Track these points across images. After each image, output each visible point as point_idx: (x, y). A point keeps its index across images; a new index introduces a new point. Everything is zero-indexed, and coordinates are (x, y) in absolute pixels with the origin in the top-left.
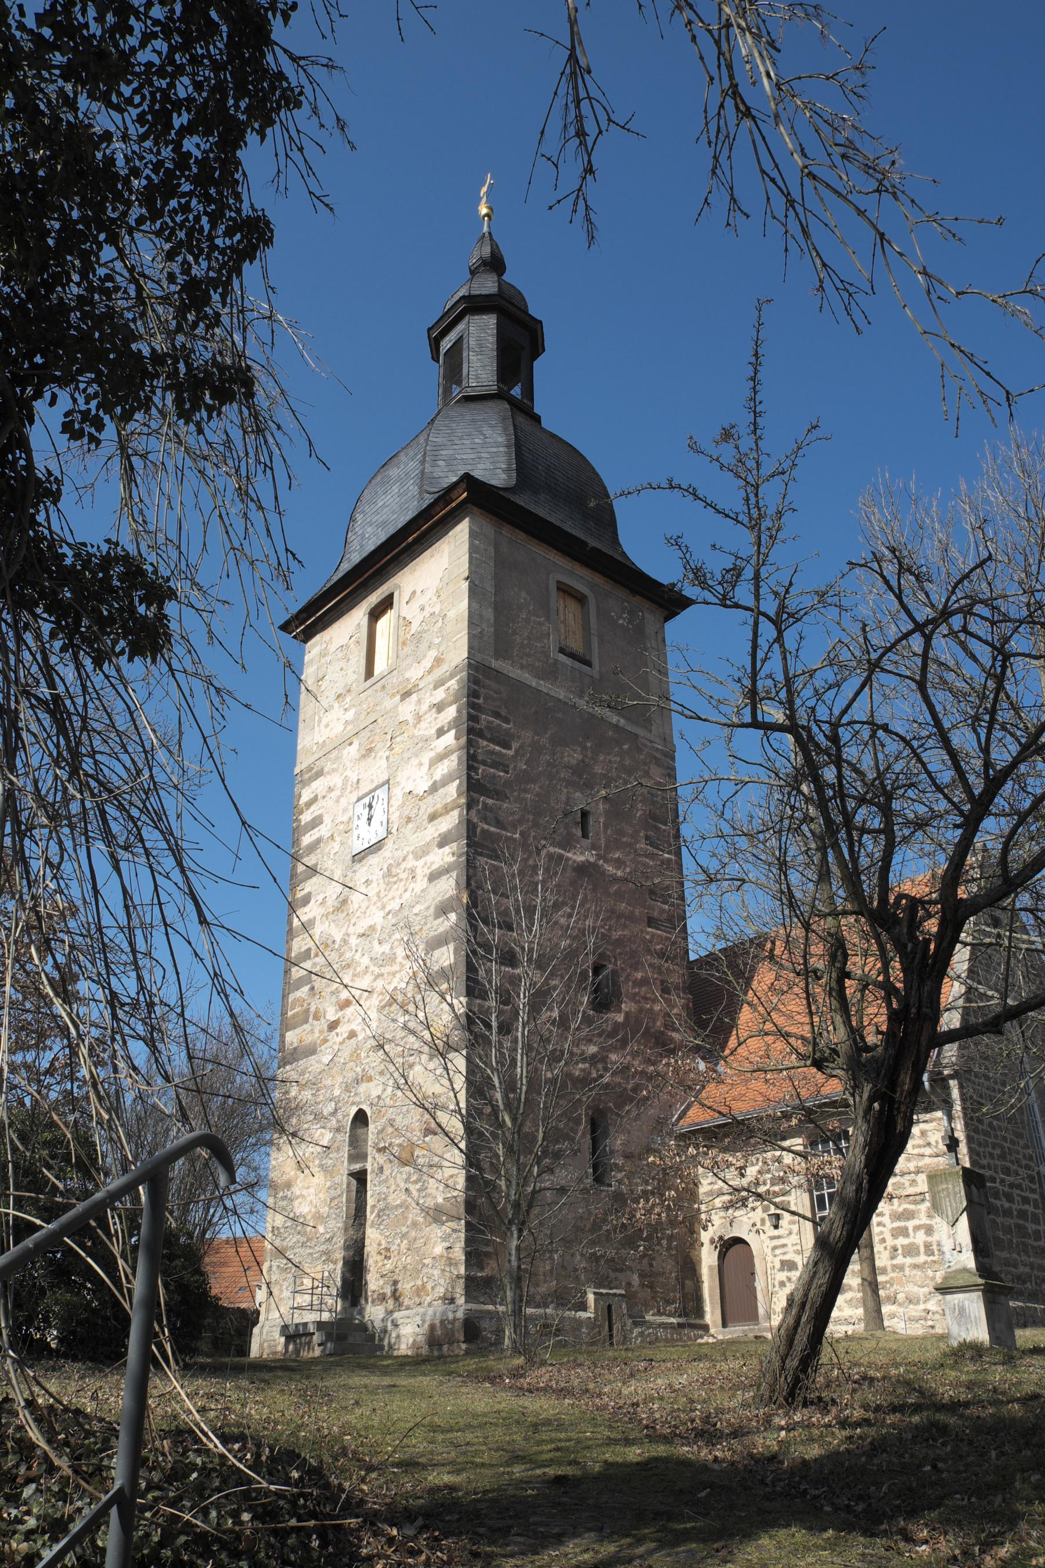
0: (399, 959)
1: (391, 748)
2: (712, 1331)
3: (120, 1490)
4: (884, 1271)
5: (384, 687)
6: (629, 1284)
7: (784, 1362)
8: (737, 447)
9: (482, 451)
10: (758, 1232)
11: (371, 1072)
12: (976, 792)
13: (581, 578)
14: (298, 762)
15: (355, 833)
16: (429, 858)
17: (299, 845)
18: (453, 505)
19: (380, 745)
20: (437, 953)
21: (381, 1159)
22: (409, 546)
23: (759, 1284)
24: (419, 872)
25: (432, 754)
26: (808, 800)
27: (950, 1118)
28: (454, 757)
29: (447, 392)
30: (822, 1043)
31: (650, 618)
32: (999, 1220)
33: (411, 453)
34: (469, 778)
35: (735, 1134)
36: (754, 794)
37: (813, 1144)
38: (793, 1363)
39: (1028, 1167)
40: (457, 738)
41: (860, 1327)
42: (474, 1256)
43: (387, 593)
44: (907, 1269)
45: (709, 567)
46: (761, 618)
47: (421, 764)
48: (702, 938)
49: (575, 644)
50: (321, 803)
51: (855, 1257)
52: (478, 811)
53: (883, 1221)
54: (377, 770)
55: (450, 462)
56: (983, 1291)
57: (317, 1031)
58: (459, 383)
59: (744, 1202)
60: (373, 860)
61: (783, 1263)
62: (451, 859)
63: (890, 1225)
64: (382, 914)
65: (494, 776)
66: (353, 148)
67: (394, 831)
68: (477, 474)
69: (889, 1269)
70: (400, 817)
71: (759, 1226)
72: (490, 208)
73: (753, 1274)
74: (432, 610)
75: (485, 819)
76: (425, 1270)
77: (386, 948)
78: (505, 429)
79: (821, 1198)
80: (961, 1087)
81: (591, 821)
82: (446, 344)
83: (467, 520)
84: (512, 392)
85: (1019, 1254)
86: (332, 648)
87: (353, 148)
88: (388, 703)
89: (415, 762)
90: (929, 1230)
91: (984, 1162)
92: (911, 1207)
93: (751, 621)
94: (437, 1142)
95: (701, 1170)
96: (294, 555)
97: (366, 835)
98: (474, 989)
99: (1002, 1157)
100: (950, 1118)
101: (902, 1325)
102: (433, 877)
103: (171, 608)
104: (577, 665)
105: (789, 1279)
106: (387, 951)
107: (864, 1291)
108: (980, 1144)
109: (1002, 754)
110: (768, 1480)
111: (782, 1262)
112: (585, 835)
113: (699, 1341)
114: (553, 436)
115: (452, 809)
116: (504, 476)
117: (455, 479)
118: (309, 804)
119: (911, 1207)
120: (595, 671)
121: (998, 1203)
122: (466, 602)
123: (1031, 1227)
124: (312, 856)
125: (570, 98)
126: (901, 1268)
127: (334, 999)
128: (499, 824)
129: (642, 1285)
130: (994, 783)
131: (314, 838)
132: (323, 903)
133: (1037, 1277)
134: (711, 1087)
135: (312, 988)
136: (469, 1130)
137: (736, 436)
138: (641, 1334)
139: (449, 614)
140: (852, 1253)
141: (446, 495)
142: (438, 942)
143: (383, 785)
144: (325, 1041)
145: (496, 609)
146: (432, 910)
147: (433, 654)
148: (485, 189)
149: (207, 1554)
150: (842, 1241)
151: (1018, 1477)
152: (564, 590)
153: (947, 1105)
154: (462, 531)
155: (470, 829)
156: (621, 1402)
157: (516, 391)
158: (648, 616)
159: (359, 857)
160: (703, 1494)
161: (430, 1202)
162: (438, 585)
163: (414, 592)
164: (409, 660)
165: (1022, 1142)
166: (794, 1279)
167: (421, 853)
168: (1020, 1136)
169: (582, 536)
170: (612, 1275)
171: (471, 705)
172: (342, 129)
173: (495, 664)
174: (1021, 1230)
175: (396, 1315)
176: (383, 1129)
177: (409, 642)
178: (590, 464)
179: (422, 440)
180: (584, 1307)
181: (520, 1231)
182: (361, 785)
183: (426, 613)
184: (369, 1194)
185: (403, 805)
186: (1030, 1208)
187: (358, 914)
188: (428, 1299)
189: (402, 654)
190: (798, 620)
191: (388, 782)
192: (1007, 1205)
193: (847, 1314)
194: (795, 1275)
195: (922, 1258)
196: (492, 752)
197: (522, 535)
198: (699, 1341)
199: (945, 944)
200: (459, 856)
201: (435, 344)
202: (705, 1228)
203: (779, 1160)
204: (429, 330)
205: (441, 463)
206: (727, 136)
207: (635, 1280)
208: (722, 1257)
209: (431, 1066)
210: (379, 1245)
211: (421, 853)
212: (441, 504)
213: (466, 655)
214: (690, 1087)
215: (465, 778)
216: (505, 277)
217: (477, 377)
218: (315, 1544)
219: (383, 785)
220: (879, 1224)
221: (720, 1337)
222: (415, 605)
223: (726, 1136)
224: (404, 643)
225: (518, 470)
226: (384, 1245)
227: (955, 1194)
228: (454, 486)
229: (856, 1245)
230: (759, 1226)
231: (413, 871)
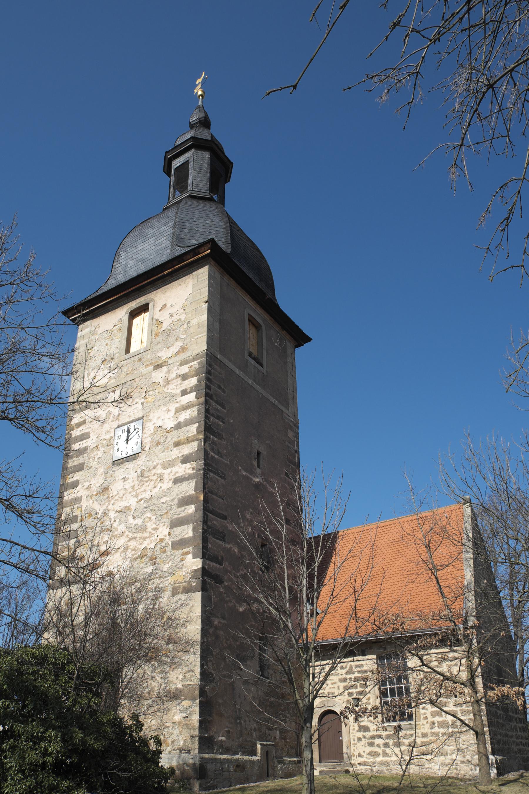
0: (149, 530)
1: (145, 398)
5: (140, 360)
6: (275, 738)
16: (175, 469)
18: (200, 256)
22: (164, 276)
24: (166, 477)
25: (178, 405)
34: (206, 423)
40: (197, 397)
42: (204, 723)
43: (144, 303)
47: (168, 410)
49: (255, 352)
50: (88, 425)
60: (130, 465)
62: (191, 472)
64: (136, 500)
65: (217, 424)
67: (147, 449)
69: (429, 734)
70: (152, 441)
72: (203, 91)
74: (179, 318)
75: (212, 450)
77: (139, 521)
81: (261, 457)
82: (177, 163)
86: (100, 331)
88: (144, 370)
97: (124, 449)
102: (177, 481)
104: (257, 365)
106: (140, 523)
112: (259, 466)
115: (193, 441)
118: (78, 425)
120: (265, 370)
128: (219, 454)
129: (281, 738)
132: (89, 488)
139: (192, 322)
141: (195, 250)
143: (138, 419)
145: (220, 324)
146: (176, 502)
147: (179, 344)
148: (200, 80)
152: (252, 321)
158: (288, 343)
163: (165, 305)
164: (160, 346)
170: (267, 732)
171: (208, 379)
173: (219, 356)
180: (254, 753)
183: (175, 318)
185: (153, 434)
187: (117, 498)
191: (142, 418)
196: (217, 410)
197: (233, 283)
201: (168, 163)
204: (166, 152)
205: (186, 230)
215: (203, 423)
219: (138, 419)
222: (166, 313)
224: (156, 335)
225: (232, 244)
228: (201, 245)
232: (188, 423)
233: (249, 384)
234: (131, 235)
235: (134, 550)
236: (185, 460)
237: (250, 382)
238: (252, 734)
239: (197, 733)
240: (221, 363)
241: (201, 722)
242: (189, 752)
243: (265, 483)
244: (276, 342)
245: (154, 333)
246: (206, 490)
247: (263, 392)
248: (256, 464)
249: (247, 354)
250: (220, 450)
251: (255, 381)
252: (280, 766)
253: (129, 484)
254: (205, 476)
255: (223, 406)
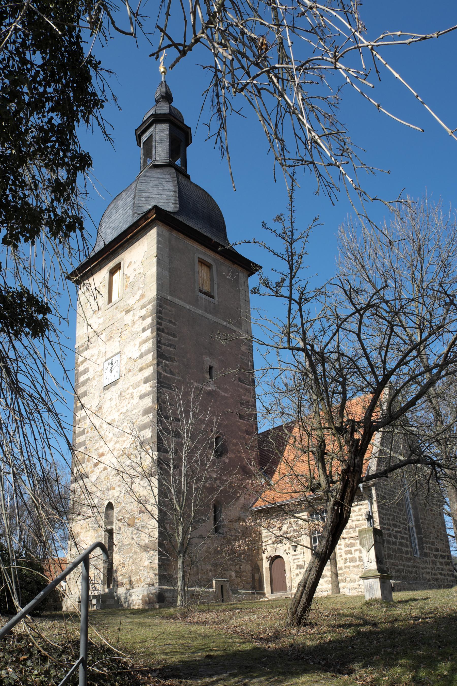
2: (267, 595)
3: (82, 658)
4: (341, 569)
5: (117, 308)
6: (231, 576)
7: (296, 609)
8: (283, 225)
9: (162, 194)
10: (287, 553)
11: (114, 486)
12: (380, 381)
13: (209, 256)
14: (77, 342)
15: (105, 376)
16: (140, 388)
17: (78, 381)
18: (149, 220)
19: (115, 335)
20: (143, 432)
21: (120, 524)
23: (288, 575)
25: (140, 340)
26: (311, 380)
27: (372, 503)
28: (151, 342)
29: (145, 162)
30: (314, 482)
31: (241, 275)
32: (391, 547)
33: (128, 194)
35: (277, 511)
36: (289, 374)
37: (312, 515)
38: (300, 609)
39: (404, 524)
40: (152, 333)
41: (330, 593)
43: (118, 262)
44: (351, 568)
45: (270, 280)
46: (293, 302)
48: (264, 426)
49: (207, 288)
51: (328, 562)
52: (162, 367)
53: (341, 548)
54: (114, 347)
55: (147, 198)
56: (380, 578)
57: (89, 467)
58: (151, 158)
59: (281, 542)
60: (113, 389)
61: (298, 566)
62: (150, 389)
63: (344, 549)
64: (118, 414)
66: (120, 109)
67: (123, 375)
68: (160, 205)
69: (343, 568)
70: (126, 369)
71: (287, 551)
72: (165, 68)
73: (285, 571)
75: (165, 371)
76: (140, 572)
78: (173, 183)
79: (315, 538)
80: (376, 490)
81: (214, 370)
83: (156, 228)
84: (176, 163)
85: (399, 561)
87: (120, 109)
89: (132, 343)
90: (360, 552)
91: (385, 522)
92: (354, 541)
93: (288, 303)
94: (145, 516)
95: (262, 528)
96: (99, 292)
98: (161, 448)
99: (393, 519)
100: (372, 503)
101: (348, 591)
103: (49, 316)
104: (207, 298)
105: (300, 573)
107: (332, 577)
108: (384, 515)
109: (391, 365)
110: (289, 654)
111: (297, 566)
112: (211, 377)
113: (261, 600)
114: (197, 186)
115: (150, 366)
116: (173, 206)
117: (150, 207)
119: (354, 541)
121: (391, 539)
122: (155, 268)
123: (404, 549)
124: (84, 387)
125: (215, 94)
126: (348, 567)
127: (96, 453)
128: (171, 373)
129: (236, 576)
130: (387, 376)
131: (85, 378)
133: (406, 570)
134: (267, 492)
135: (86, 448)
136: (160, 511)
137: (283, 220)
138: (236, 597)
140: (327, 562)
141: (145, 216)
142: (143, 427)
143: (117, 354)
144: (93, 471)
145: (169, 271)
147: (140, 292)
149: (96, 681)
150: (324, 557)
151: (383, 650)
152: (201, 262)
153: (370, 498)
154: (153, 233)
155: (159, 376)
156: (230, 626)
157: (178, 163)
158: (241, 275)
159: (106, 388)
160: (264, 659)
161: (142, 543)
162: (142, 259)
163: (131, 262)
165: (402, 513)
166: (302, 573)
167: (136, 386)
168: (401, 510)
169: (210, 237)
170: (223, 572)
171: (158, 317)
172: (115, 100)
173: (169, 298)
174: (400, 551)
175: (131, 591)
176: (120, 511)
177: (129, 286)
178: (214, 200)
179: (133, 187)
180: (212, 587)
181: (184, 556)
182: (107, 354)
183: (137, 272)
184: (114, 539)
185: (127, 364)
186: (404, 541)
187: (107, 414)
188: (142, 584)
189: (125, 292)
190: (308, 301)
191: (120, 352)
192: (394, 540)
193: (324, 588)
194: (303, 571)
195: (358, 563)
196: (169, 340)
197: (181, 236)
198: (261, 600)
199: (365, 442)
200: (153, 388)
201: (139, 138)
202: (264, 553)
203: (296, 523)
204: (136, 130)
205: (143, 199)
206: (281, 116)
207: (233, 574)
208: (271, 564)
209: (142, 483)
210: (120, 561)
211: (136, 386)
212: (143, 220)
213: (156, 294)
214: (258, 492)
215: (156, 351)
216: (172, 104)
217: (160, 155)
218: (127, 678)
219: (117, 354)
220: (339, 549)
221: (270, 598)
222: (131, 268)
223: (273, 512)
226: (122, 561)
227: (370, 539)
228: (149, 211)
229: (329, 558)
230: (287, 551)
231: (132, 394)
232: (147, 353)
233: (199, 315)
234: (110, 207)
235: (119, 450)
236: (146, 381)
237: (200, 312)
238: (208, 574)
239: (157, 572)
240: (171, 303)
241: (159, 565)
242: (153, 585)
243: (218, 390)
244: (228, 275)
245: (125, 285)
246: (160, 402)
247: (214, 318)
248: (208, 376)
249: (197, 291)
250: (172, 370)
251: (206, 311)
252: (234, 596)
253: (114, 403)
254: (158, 391)
255: (174, 336)
